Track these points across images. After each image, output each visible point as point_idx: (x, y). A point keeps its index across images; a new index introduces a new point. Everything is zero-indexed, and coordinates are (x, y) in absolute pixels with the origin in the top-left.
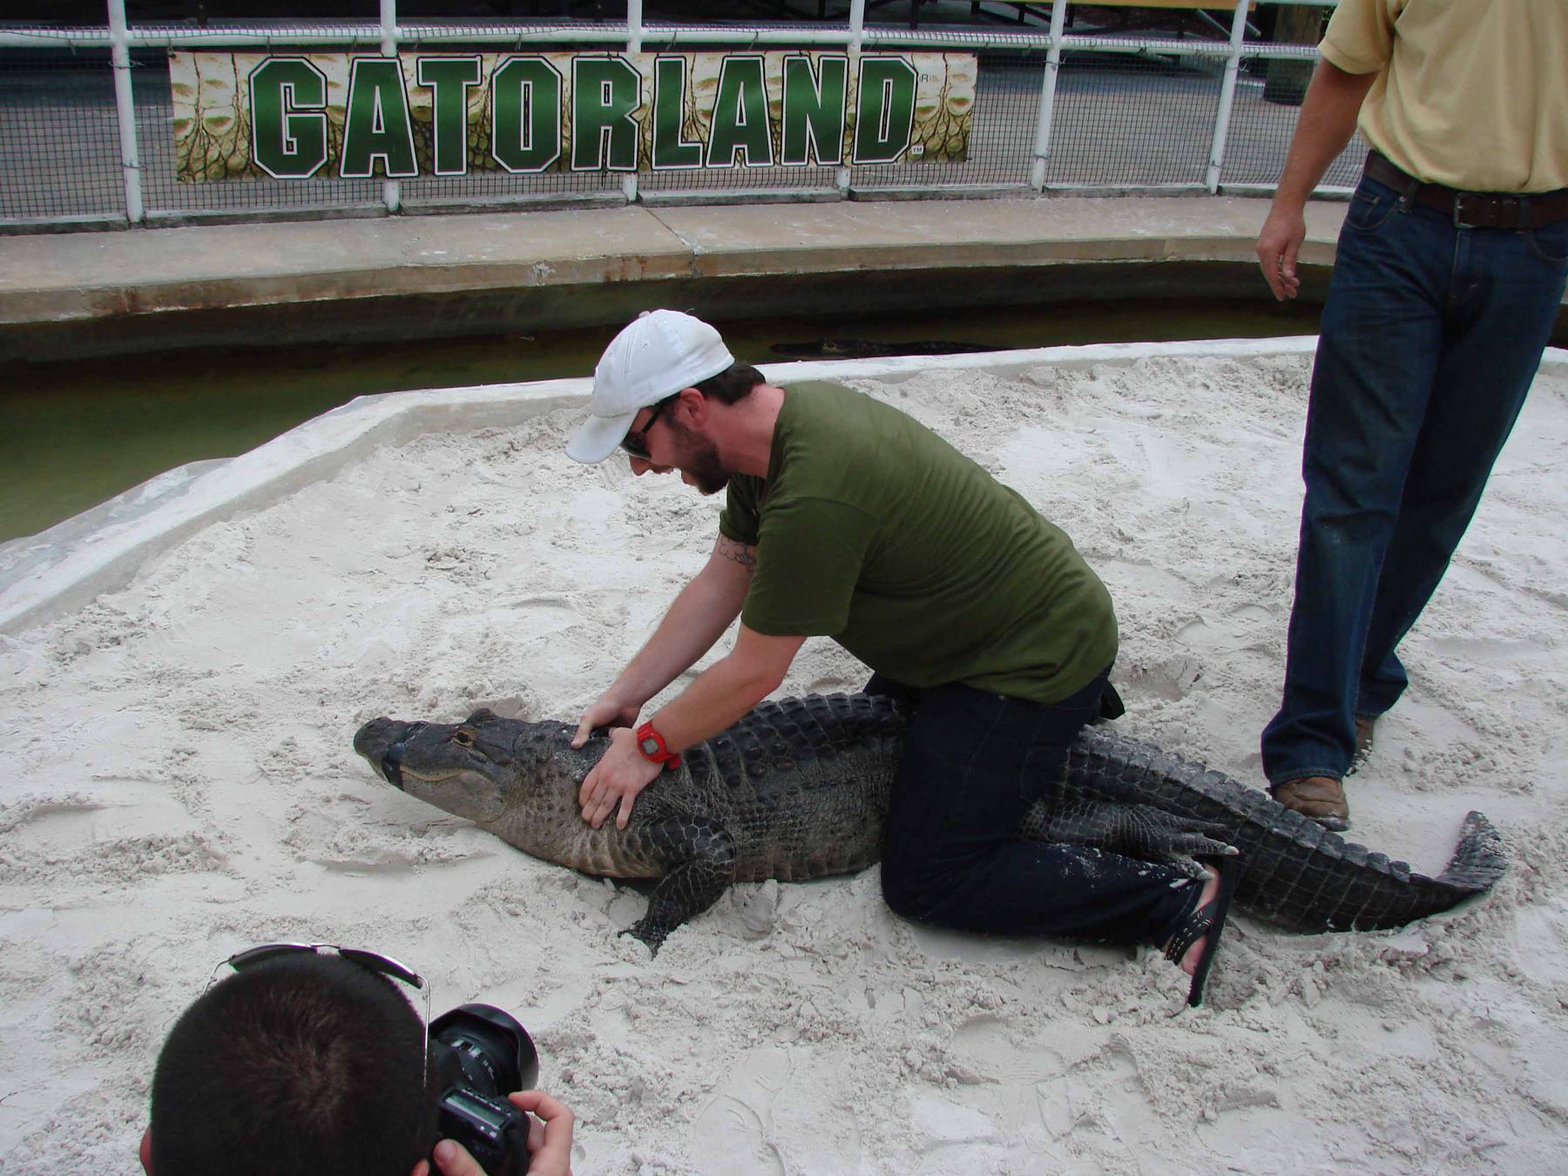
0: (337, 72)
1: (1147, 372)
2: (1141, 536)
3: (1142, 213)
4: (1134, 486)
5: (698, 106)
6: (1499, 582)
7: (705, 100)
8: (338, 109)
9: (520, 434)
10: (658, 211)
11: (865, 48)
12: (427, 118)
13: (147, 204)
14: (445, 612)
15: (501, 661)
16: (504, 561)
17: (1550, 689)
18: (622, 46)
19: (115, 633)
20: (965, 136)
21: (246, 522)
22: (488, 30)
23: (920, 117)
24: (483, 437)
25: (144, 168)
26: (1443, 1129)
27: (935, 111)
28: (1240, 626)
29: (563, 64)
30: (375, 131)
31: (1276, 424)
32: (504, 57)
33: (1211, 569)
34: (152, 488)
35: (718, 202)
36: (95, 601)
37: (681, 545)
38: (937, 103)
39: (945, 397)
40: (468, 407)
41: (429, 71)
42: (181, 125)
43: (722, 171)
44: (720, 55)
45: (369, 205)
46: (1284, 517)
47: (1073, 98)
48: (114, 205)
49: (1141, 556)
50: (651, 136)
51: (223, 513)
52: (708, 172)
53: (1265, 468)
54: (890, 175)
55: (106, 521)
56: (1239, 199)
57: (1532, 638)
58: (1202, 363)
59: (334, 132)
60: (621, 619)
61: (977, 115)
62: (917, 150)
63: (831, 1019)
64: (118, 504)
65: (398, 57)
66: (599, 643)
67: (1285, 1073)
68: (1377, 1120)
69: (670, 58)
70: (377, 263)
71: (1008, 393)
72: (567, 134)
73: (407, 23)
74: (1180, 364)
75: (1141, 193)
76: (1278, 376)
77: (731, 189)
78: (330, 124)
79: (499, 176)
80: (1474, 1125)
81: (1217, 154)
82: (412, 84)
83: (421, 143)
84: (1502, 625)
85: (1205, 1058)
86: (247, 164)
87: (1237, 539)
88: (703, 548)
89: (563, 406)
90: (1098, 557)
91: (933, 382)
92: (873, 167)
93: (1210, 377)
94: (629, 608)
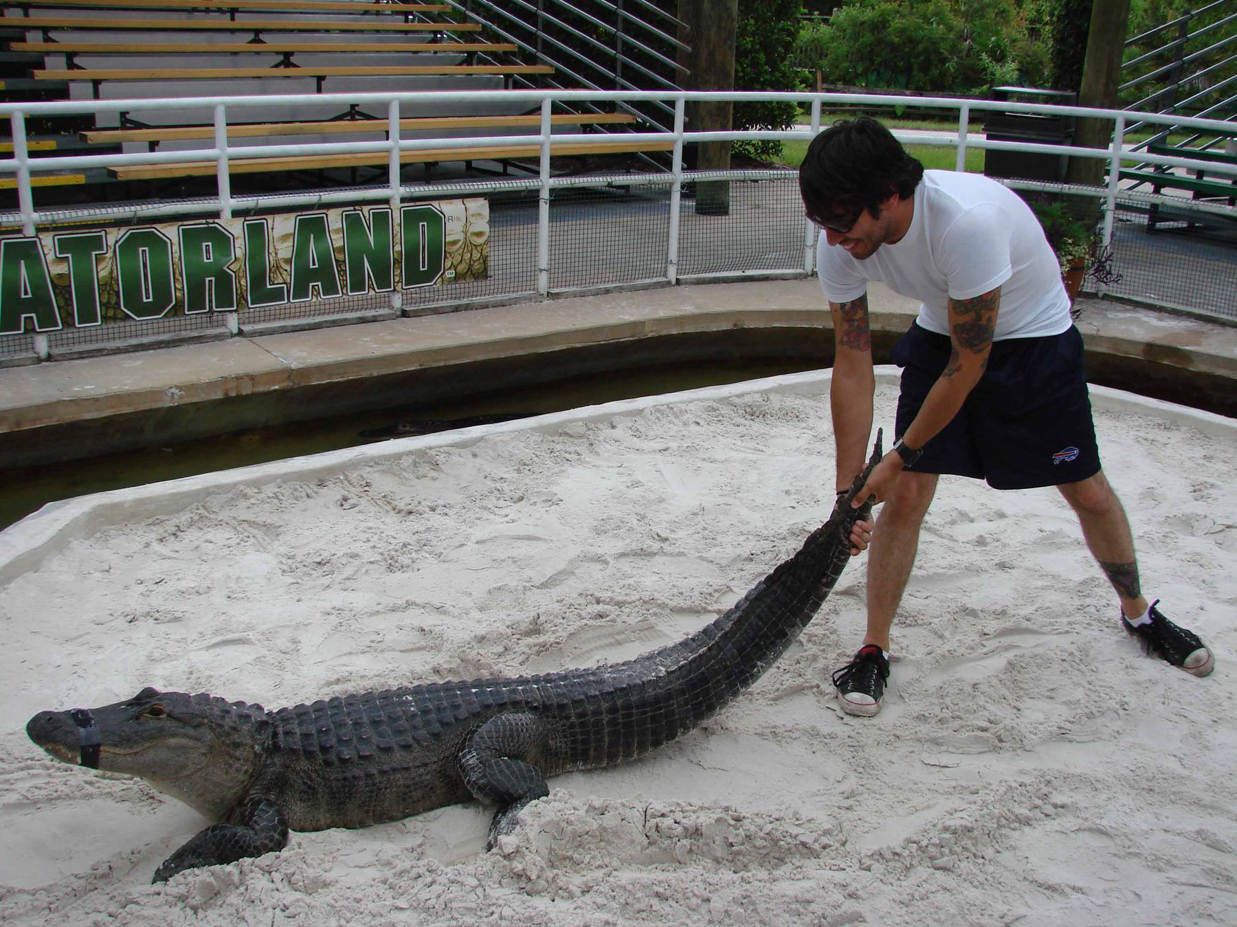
1: (653, 418)
2: (671, 536)
3: (624, 304)
4: (661, 500)
5: (280, 256)
7: (285, 250)
9: (183, 519)
10: (258, 339)
11: (403, 200)
12: (65, 283)
14: (152, 660)
16: (192, 616)
18: (216, 215)
20: (485, 260)
22: (109, 210)
26: (982, 915)
27: (460, 243)
29: (171, 232)
31: (753, 444)
32: (123, 230)
33: (731, 552)
35: (302, 329)
37: (328, 587)
38: (461, 237)
39: (506, 454)
40: (140, 502)
41: (64, 245)
43: (303, 305)
44: (293, 215)
45: (24, 355)
46: (774, 508)
49: (677, 550)
50: (246, 282)
52: (293, 306)
53: (753, 476)
54: (432, 295)
56: (693, 286)
58: (691, 407)
60: (294, 647)
62: (450, 274)
63: (526, 915)
65: (37, 236)
67: (865, 896)
68: (936, 917)
69: (253, 220)
70: (38, 401)
72: (179, 286)
73: (42, 210)
74: (675, 409)
75: (621, 289)
76: (748, 409)
79: (127, 324)
80: (1003, 908)
81: (673, 255)
82: (51, 257)
83: (62, 304)
84: (943, 563)
85: (809, 896)
87: (744, 529)
88: (346, 587)
89: (214, 493)
90: (646, 555)
91: (495, 443)
93: (699, 416)
94: (299, 638)
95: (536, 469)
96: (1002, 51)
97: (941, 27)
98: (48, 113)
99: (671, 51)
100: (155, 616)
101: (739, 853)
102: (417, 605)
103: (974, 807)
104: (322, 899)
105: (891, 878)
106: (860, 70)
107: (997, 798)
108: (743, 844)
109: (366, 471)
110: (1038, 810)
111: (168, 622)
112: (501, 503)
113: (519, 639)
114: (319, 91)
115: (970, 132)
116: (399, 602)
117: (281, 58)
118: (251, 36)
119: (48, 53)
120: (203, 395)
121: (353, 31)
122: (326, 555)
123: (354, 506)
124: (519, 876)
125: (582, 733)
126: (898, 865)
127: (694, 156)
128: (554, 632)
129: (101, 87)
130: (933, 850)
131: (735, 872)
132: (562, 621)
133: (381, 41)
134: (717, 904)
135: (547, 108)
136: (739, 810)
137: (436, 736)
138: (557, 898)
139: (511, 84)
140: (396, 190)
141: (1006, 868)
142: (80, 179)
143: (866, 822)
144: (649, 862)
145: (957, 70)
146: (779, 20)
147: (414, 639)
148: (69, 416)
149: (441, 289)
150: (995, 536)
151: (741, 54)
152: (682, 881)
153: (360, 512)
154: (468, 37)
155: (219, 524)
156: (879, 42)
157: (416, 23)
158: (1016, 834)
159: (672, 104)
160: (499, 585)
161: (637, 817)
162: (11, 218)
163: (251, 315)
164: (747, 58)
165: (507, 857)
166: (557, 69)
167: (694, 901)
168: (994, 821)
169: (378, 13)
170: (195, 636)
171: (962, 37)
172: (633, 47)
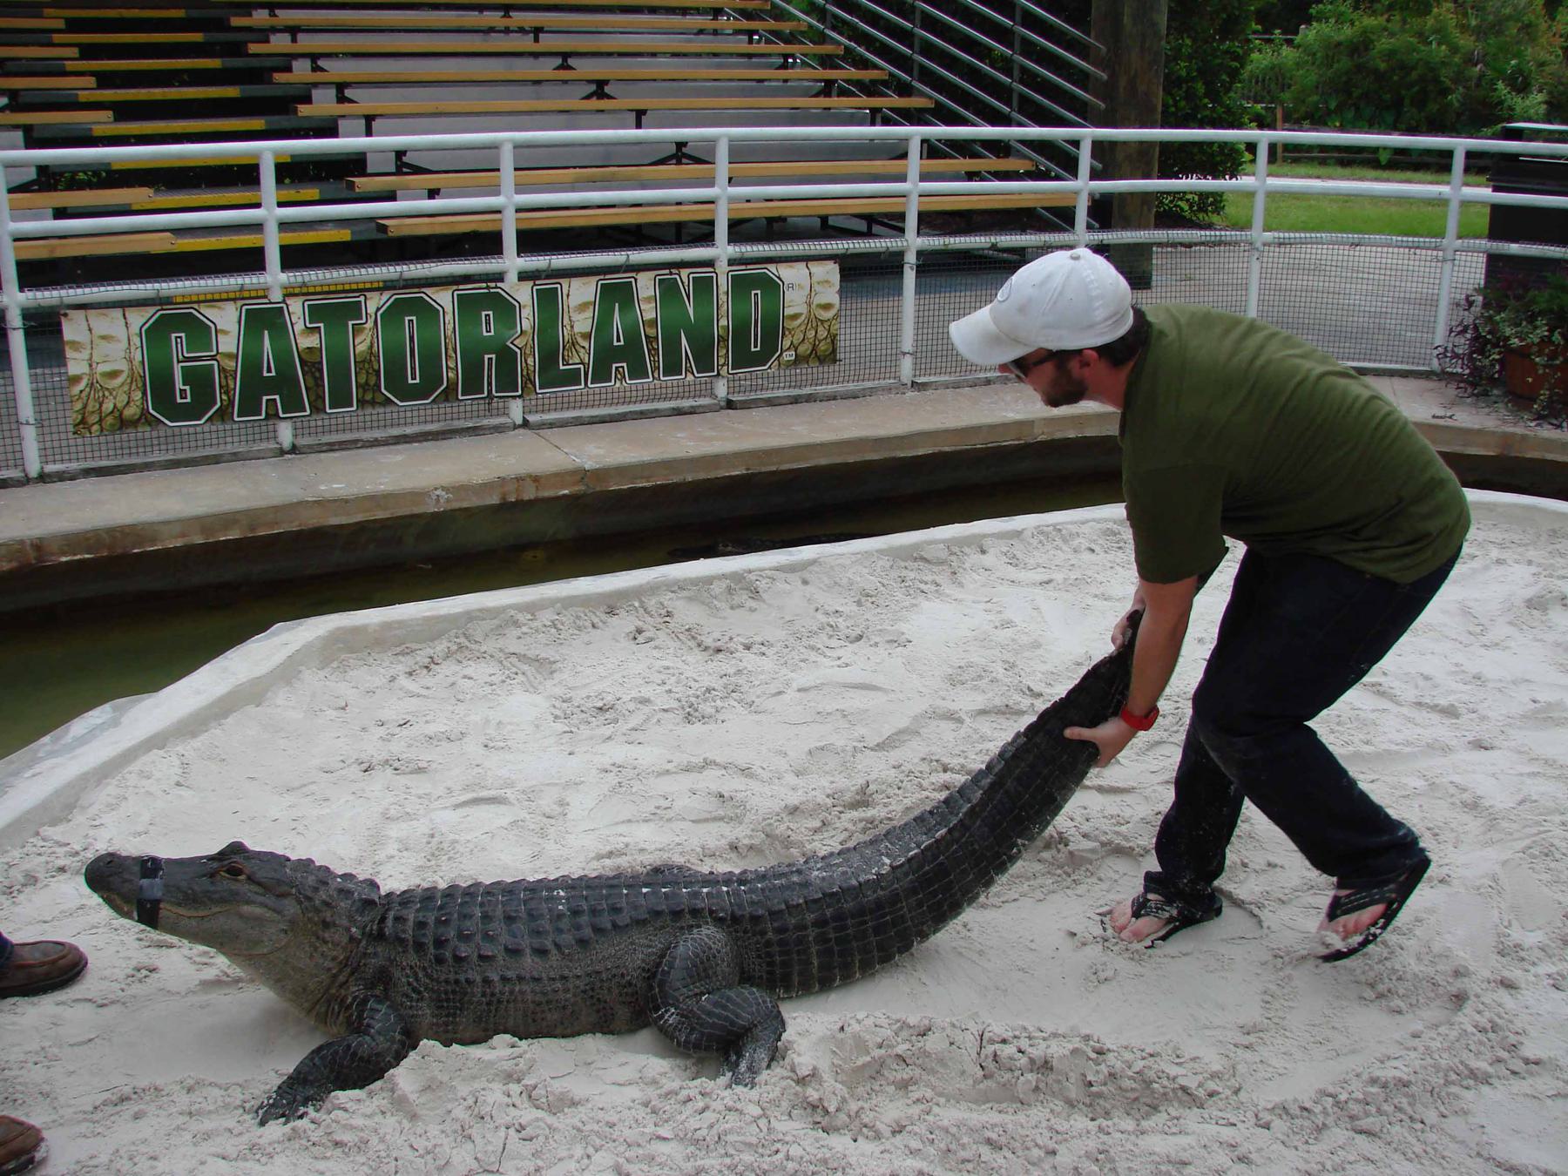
0: (227, 321)
1: (1034, 542)
3: (1008, 398)
4: (1036, 645)
5: (576, 330)
6: (1392, 700)
7: (583, 323)
8: (229, 356)
10: (547, 432)
11: (731, 262)
13: (44, 459)
15: (449, 859)
17: (1452, 790)
18: (499, 277)
19: (60, 863)
20: (833, 339)
21: (180, 749)
22: (370, 270)
23: (790, 325)
24: (402, 654)
25: (40, 424)
27: (803, 317)
28: (1155, 762)
29: (444, 299)
30: (265, 374)
34: (79, 726)
36: (38, 834)
37: (609, 738)
38: (803, 309)
39: (845, 581)
40: (387, 626)
41: (316, 313)
42: (76, 380)
43: (604, 390)
44: (594, 279)
45: (264, 445)
47: (934, 300)
48: (11, 463)
50: (533, 361)
51: (157, 742)
52: (591, 391)
55: (35, 761)
57: (1428, 745)
58: (1085, 529)
59: (226, 377)
60: (559, 810)
61: (843, 319)
62: (789, 356)
63: (819, 1156)
64: (45, 745)
65: (284, 302)
66: (543, 833)
69: (545, 284)
70: (277, 500)
71: (904, 573)
72: (452, 365)
74: (1064, 532)
77: (614, 407)
78: (222, 370)
79: (388, 409)
82: (299, 327)
83: (311, 382)
85: (1185, 1156)
86: (142, 414)
88: (631, 739)
89: (477, 618)
91: (832, 567)
92: (748, 376)
95: (881, 602)
96: (1525, 78)
97: (1444, 47)
98: (338, 154)
99: (1082, 79)
100: (395, 766)
101: (1099, 1095)
102: (716, 764)
103: (1413, 1054)
104: (568, 1120)
105: (1296, 1140)
106: (1333, 105)
107: (1446, 1045)
108: (1105, 1084)
109: (667, 598)
110: (1502, 1065)
111: (411, 773)
112: (834, 643)
113: (841, 812)
114: (639, 126)
115: (1467, 184)
116: (694, 760)
117: (593, 88)
118: (559, 61)
119: (316, 85)
120: (474, 499)
121: (685, 55)
122: (609, 699)
123: (650, 640)
124: (814, 1107)
125: (781, 953)
126: (1307, 1123)
127: (1104, 212)
128: (885, 805)
129: (375, 124)
130: (1355, 1108)
131: (1093, 1119)
132: (897, 791)
133: (719, 66)
134: (1065, 1158)
135: (915, 149)
136: (1103, 1040)
137: (583, 943)
138: (860, 1139)
139: (879, 120)
140: (722, 250)
141: (1453, 1138)
142: (345, 235)
143: (1269, 1065)
144: (983, 1099)
145: (1463, 104)
146: (1222, 40)
147: (712, 806)
148: (313, 520)
149: (777, 374)
150: (1471, 706)
151: (1172, 83)
152: (1022, 1127)
153: (656, 648)
154: (827, 61)
155: (481, 657)
156: (1359, 68)
157: (762, 44)
158: (1469, 1095)
159: (1076, 143)
160: (822, 744)
161: (970, 1041)
162: (255, 280)
163: (540, 402)
164: (1180, 88)
165: (801, 1081)
166: (937, 103)
167: (1036, 1152)
168: (1441, 1074)
169: (715, 32)
170: (441, 791)
171: (1470, 61)
172: (1035, 75)
